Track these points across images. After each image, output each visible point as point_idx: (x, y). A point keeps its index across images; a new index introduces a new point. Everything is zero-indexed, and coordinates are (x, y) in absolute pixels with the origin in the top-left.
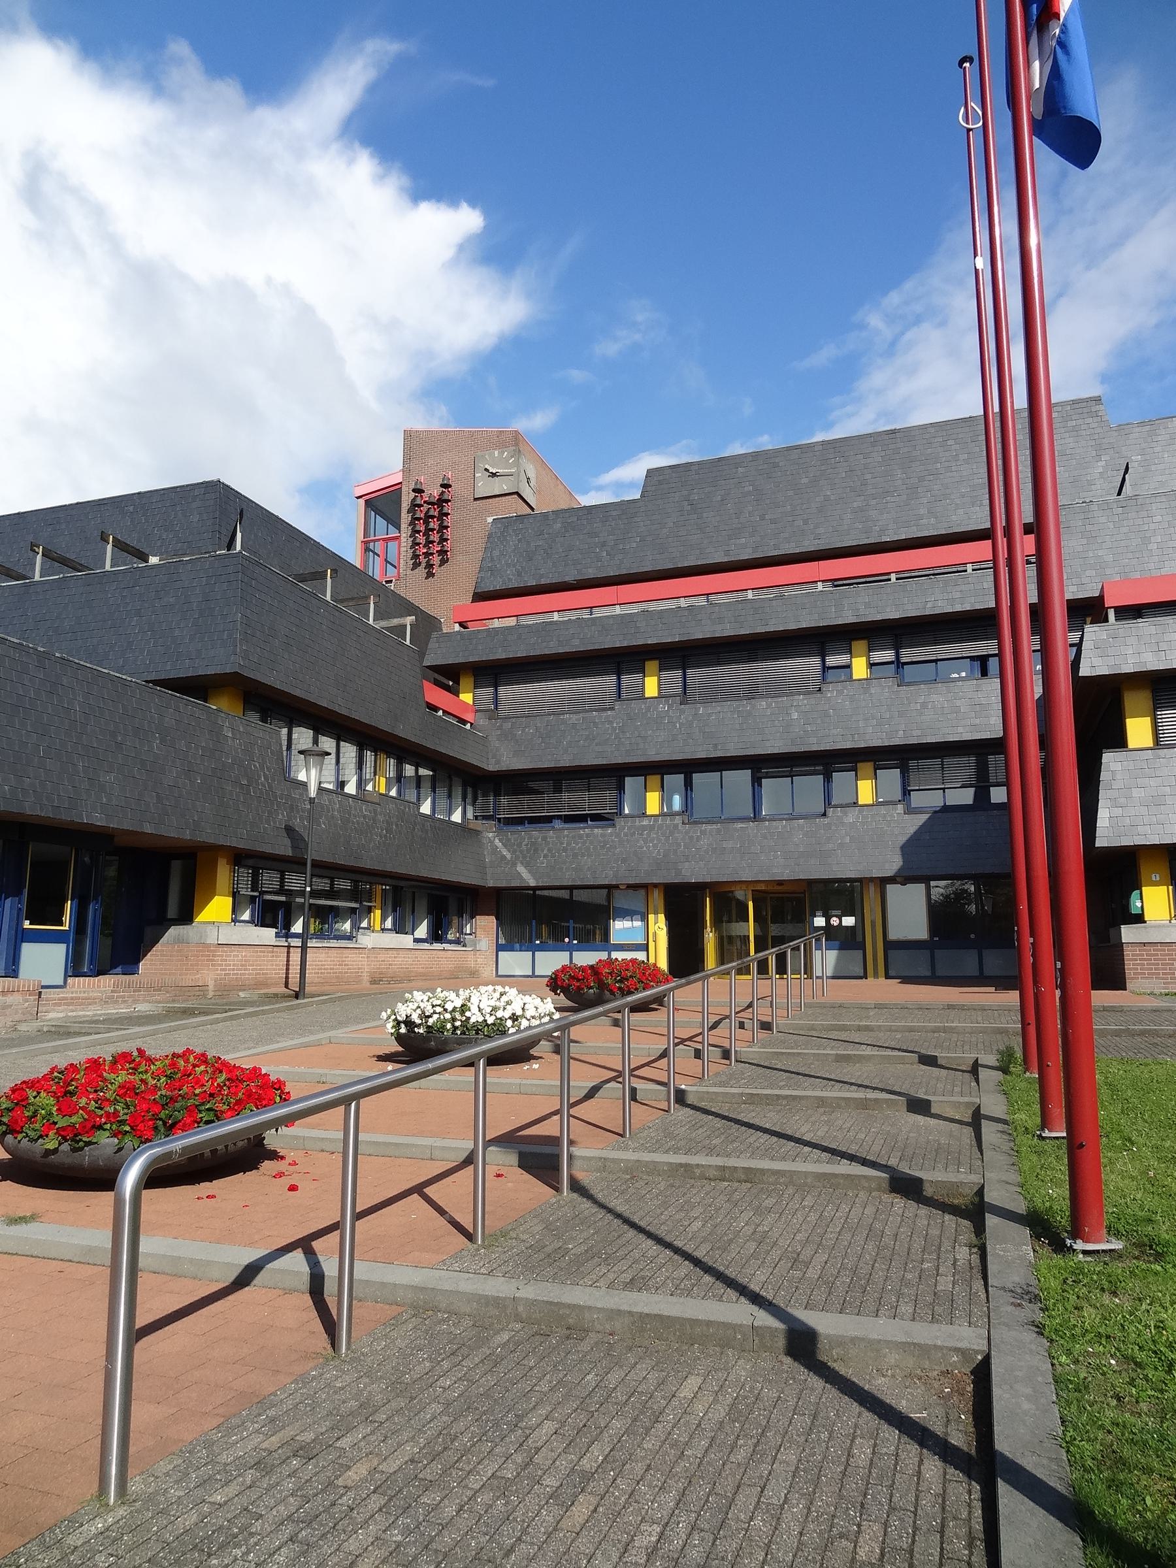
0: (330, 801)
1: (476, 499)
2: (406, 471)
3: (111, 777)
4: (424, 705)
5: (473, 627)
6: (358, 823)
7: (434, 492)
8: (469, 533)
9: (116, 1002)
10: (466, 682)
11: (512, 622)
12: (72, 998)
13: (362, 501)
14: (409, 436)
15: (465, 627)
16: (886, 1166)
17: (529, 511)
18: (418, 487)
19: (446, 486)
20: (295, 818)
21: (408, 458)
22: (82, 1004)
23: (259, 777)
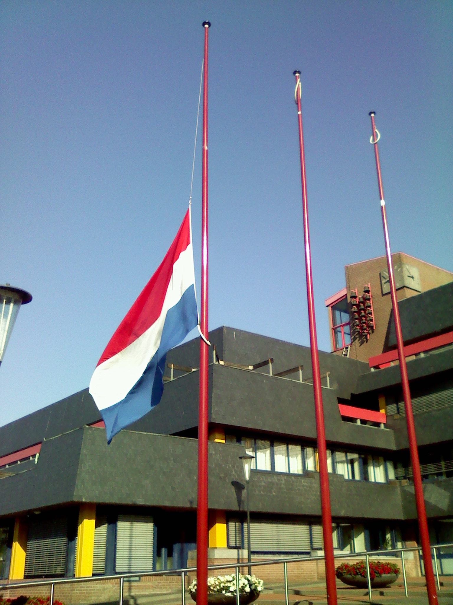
0: (279, 480)
1: (383, 295)
2: (348, 288)
3: (147, 482)
4: (340, 418)
5: (382, 368)
6: (299, 489)
7: (360, 295)
8: (380, 313)
9: (161, 588)
10: (382, 401)
11: (413, 358)
12: (138, 586)
13: (330, 308)
14: (347, 268)
15: (379, 368)
16: (427, 585)
17: (419, 293)
18: (354, 295)
19: (368, 292)
20: (255, 491)
21: (348, 279)
22: (143, 589)
23: (232, 472)
